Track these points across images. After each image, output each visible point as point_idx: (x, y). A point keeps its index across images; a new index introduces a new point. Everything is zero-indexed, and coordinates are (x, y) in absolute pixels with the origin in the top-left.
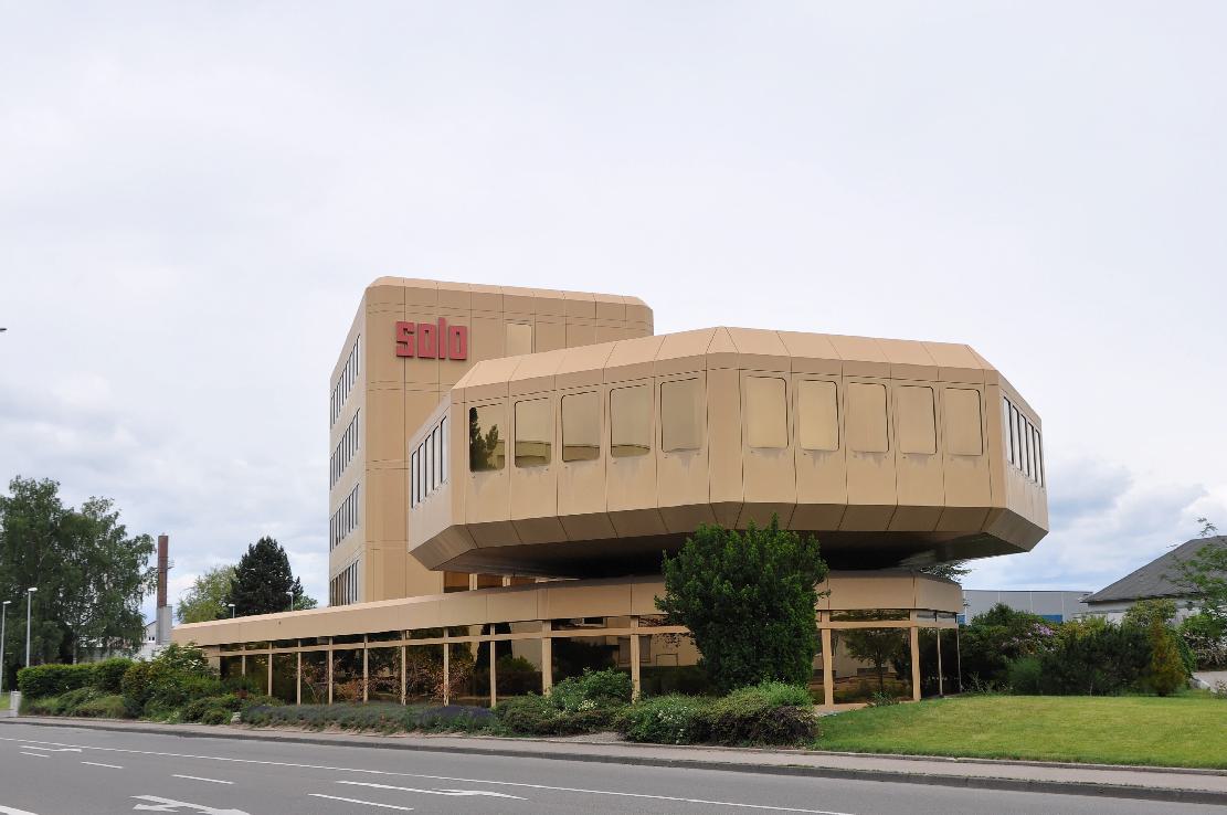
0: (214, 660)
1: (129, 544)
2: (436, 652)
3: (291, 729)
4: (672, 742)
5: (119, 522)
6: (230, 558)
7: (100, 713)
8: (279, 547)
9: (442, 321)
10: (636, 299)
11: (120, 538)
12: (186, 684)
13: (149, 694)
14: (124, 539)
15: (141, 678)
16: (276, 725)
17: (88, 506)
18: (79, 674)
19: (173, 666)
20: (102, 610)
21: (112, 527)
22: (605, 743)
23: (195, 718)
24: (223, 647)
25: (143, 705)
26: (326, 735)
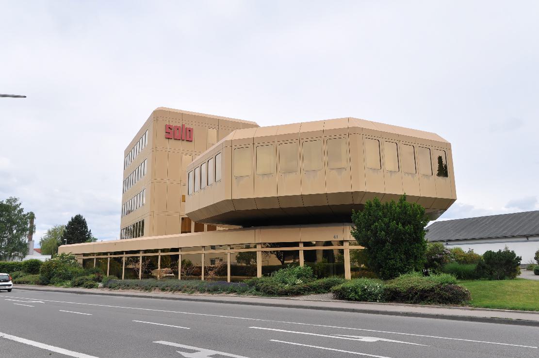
0: (80, 261)
1: (24, 215)
2: (120, 260)
3: (133, 290)
4: (375, 300)
5: (21, 207)
6: (64, 220)
7: (27, 283)
8: (83, 218)
9: (183, 125)
10: (254, 122)
11: (21, 213)
12: (70, 270)
13: (53, 275)
14: (22, 214)
15: (49, 267)
16: (123, 289)
17: (8, 201)
18: (13, 266)
19: (63, 262)
20: (10, 242)
21: (18, 209)
22: (325, 300)
23: (79, 285)
24: (84, 255)
25: (50, 279)
26: (153, 294)
